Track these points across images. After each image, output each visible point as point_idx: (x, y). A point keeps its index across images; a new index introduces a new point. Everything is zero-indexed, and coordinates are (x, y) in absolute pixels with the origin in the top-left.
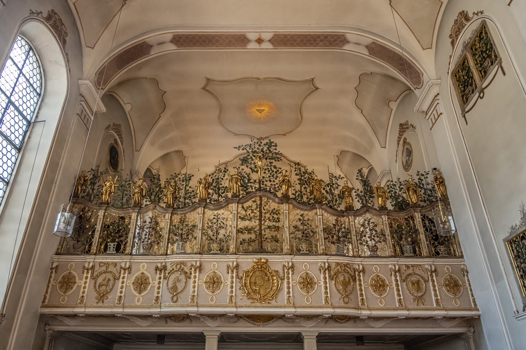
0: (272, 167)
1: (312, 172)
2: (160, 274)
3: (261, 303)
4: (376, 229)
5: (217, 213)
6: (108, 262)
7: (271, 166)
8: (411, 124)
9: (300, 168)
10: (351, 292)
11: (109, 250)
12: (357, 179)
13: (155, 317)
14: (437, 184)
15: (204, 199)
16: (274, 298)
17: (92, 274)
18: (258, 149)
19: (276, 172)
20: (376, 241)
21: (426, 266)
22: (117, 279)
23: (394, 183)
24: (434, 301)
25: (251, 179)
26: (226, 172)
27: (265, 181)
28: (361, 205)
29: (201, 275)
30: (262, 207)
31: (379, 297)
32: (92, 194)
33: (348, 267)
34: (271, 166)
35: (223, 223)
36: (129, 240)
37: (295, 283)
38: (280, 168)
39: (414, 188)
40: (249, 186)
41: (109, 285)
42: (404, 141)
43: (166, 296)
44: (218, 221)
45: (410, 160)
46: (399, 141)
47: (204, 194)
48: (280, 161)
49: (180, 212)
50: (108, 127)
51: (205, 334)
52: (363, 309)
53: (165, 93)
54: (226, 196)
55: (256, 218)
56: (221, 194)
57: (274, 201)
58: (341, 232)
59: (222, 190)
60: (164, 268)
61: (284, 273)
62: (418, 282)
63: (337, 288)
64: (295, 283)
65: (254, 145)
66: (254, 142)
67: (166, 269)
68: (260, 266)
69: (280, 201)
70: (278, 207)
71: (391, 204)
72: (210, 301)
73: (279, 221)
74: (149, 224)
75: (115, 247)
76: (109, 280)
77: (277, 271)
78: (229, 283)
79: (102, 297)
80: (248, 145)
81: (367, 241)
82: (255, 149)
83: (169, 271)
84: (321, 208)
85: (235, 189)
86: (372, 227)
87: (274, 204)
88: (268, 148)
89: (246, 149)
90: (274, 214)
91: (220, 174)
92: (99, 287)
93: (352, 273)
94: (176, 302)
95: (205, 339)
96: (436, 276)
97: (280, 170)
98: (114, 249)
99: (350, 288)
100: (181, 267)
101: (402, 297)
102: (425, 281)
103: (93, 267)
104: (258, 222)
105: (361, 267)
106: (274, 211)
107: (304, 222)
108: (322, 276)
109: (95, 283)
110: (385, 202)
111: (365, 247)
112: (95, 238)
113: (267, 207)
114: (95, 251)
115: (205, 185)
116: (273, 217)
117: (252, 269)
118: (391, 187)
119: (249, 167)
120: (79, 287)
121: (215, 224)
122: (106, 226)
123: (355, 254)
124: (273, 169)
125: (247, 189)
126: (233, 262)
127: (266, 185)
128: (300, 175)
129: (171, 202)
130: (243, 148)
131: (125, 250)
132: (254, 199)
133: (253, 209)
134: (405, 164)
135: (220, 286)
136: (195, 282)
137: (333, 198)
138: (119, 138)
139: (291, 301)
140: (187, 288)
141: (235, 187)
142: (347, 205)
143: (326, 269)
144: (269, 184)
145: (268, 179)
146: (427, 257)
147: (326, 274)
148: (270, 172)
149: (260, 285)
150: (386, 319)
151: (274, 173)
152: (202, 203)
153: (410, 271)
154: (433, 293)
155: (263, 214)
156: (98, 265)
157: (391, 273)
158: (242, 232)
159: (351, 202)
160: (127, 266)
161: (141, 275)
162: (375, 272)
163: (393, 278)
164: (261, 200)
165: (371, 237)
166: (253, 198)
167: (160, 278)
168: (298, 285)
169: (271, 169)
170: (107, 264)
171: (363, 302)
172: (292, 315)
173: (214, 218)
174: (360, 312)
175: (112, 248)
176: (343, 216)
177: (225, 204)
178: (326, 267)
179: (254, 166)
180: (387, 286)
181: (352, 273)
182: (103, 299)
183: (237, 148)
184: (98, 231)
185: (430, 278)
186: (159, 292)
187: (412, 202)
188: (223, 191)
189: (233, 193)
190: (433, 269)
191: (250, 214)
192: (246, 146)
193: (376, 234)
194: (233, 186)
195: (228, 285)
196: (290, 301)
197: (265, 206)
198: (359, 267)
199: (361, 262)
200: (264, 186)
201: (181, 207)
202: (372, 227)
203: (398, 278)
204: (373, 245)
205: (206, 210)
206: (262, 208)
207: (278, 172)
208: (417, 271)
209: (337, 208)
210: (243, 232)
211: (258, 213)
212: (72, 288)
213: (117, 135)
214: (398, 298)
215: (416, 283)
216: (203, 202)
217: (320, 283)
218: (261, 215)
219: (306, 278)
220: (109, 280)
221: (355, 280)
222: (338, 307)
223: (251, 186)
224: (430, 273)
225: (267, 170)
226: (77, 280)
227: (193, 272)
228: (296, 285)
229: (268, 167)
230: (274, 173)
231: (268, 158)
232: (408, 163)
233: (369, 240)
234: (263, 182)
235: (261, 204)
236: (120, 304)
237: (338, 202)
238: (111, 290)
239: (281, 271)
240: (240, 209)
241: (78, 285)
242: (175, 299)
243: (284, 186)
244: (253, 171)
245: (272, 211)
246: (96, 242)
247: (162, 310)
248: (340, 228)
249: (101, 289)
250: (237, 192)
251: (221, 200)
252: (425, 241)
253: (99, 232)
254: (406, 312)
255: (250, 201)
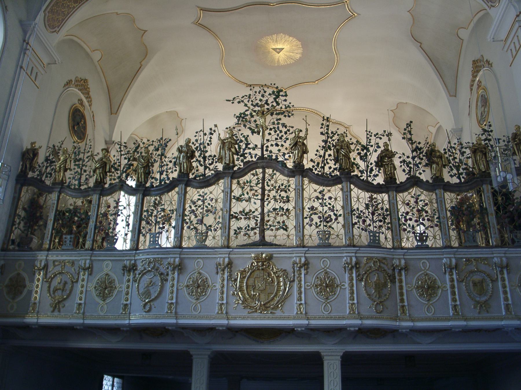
1: (344, 133)
2: (129, 276)
3: (261, 313)
5: (203, 192)
7: (278, 124)
8: (487, 60)
11: (65, 245)
13: (123, 330)
14: (516, 144)
15: (186, 173)
16: (279, 306)
17: (46, 275)
18: (261, 100)
19: (286, 133)
20: (426, 226)
21: (495, 260)
22: (74, 282)
25: (250, 144)
26: (212, 134)
27: (269, 146)
29: (181, 276)
30: (266, 182)
31: (426, 303)
32: (44, 173)
33: (384, 263)
34: (278, 124)
35: (212, 206)
36: (89, 230)
37: (310, 286)
38: (292, 127)
39: (483, 150)
40: (246, 154)
41: (66, 290)
42: (478, 85)
43: (137, 303)
44: (204, 203)
45: (486, 112)
49: (154, 193)
50: (68, 83)
52: (403, 320)
53: (145, 32)
54: (215, 168)
55: (256, 198)
56: (208, 165)
59: (209, 160)
60: (134, 267)
61: (294, 273)
62: (482, 282)
63: (367, 292)
64: (310, 286)
65: (255, 95)
66: (254, 92)
68: (261, 263)
69: (290, 174)
70: (288, 181)
71: (450, 174)
73: (288, 201)
74: (114, 209)
75: (72, 240)
76: (66, 283)
77: (285, 270)
78: (218, 286)
79: (57, 306)
80: (247, 96)
82: (256, 102)
83: (139, 272)
87: (282, 177)
88: (275, 99)
89: (243, 101)
90: (281, 191)
92: (54, 292)
93: (390, 272)
94: (149, 311)
96: (508, 273)
97: (291, 130)
98: (71, 243)
101: (458, 303)
103: (46, 267)
104: (259, 202)
105: (403, 262)
106: (281, 187)
108: (347, 275)
109: (49, 287)
111: (411, 235)
113: (272, 182)
114: (47, 246)
115: (187, 153)
116: (280, 195)
117: (249, 267)
118: (449, 150)
119: (248, 126)
121: (200, 206)
122: (61, 214)
123: (396, 244)
124: (281, 128)
125: (245, 158)
126: (224, 258)
127: (271, 152)
129: (143, 180)
130: (239, 100)
132: (254, 171)
133: (252, 185)
134: (479, 118)
135: (206, 291)
136: (173, 286)
137: (368, 166)
138: (86, 98)
140: (163, 294)
141: (227, 155)
142: (387, 176)
144: (275, 149)
145: (274, 143)
146: (497, 246)
147: (352, 273)
148: (277, 133)
149: (261, 289)
151: (283, 134)
152: (183, 179)
154: (502, 296)
155: (266, 192)
157: (445, 271)
160: (87, 265)
162: (423, 268)
163: (447, 276)
164: (264, 173)
165: (419, 220)
166: (252, 170)
167: (129, 281)
168: (313, 288)
169: (278, 128)
170: (63, 263)
171: (403, 310)
173: (199, 199)
174: (398, 324)
175: (68, 241)
179: (254, 126)
181: (390, 272)
182: (59, 306)
183: (230, 101)
184: (51, 220)
185: (499, 276)
188: (210, 162)
189: (225, 163)
191: (249, 192)
192: (243, 97)
193: (426, 216)
197: (269, 180)
198: (400, 262)
200: (269, 152)
201: (155, 186)
202: (421, 206)
203: (454, 277)
204: (422, 232)
205: (188, 189)
206: (266, 184)
207: (288, 133)
208: (482, 267)
209: (373, 180)
210: (238, 217)
211: (260, 191)
213: (83, 94)
214: (453, 303)
215: (479, 283)
216: (184, 177)
217: (343, 285)
218: (263, 194)
219: (325, 279)
220: (66, 283)
221: (393, 281)
222: (368, 318)
223: (250, 153)
224: (500, 269)
225: (273, 130)
227: (170, 273)
228: (311, 288)
229: (274, 126)
230: (283, 134)
231: (275, 113)
233: (415, 224)
234: (267, 147)
235: (264, 178)
236: (79, 313)
237: (373, 173)
238: (68, 296)
239: (290, 270)
240: (234, 186)
242: (147, 308)
243: (297, 151)
245: (279, 187)
246: (48, 234)
248: (374, 209)
249: (56, 294)
251: (208, 174)
253: (52, 222)
254: (463, 323)
255: (249, 174)
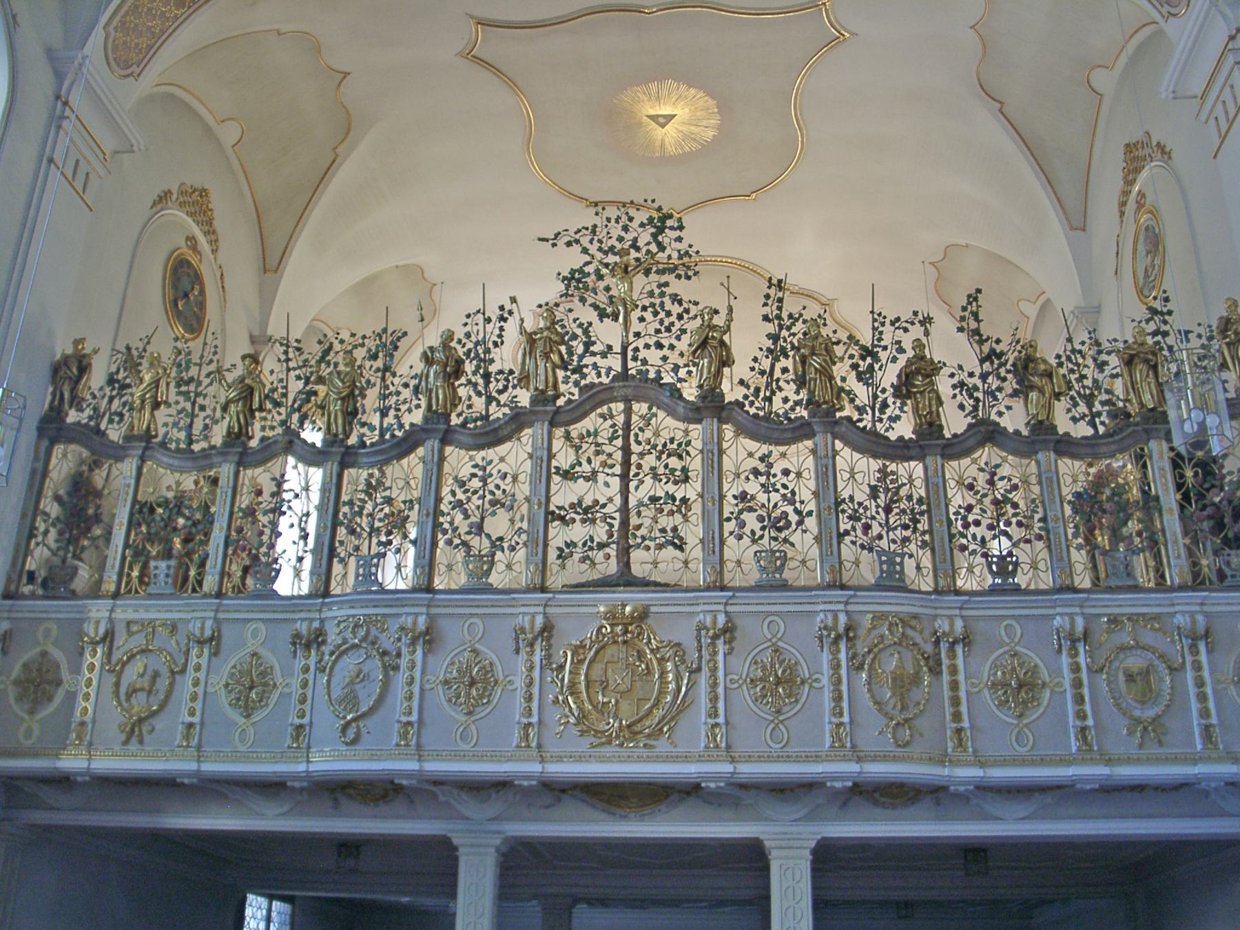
0: (667, 300)
1: (820, 316)
3: (621, 745)
4: (1015, 500)
5: (483, 459)
6: (152, 621)
7: (662, 294)
8: (1158, 144)
9: (780, 300)
10: (921, 707)
11: (155, 583)
12: (961, 330)
14: (1228, 344)
15: (442, 414)
16: (665, 729)
17: (109, 655)
18: (620, 239)
19: (680, 317)
20: (1015, 539)
21: (1179, 619)
22: (177, 672)
23: (1078, 347)
24: (1197, 731)
25: (594, 343)
28: (969, 420)
29: (430, 658)
30: (632, 433)
35: (504, 491)
37: (737, 681)
38: (696, 304)
40: (587, 366)
42: (1137, 202)
43: (326, 721)
44: (485, 484)
46: (1123, 204)
47: (441, 397)
48: (693, 278)
49: (366, 460)
51: (455, 841)
54: (512, 402)
55: (610, 471)
56: (494, 394)
57: (671, 413)
58: (896, 511)
59: (498, 381)
60: (318, 637)
61: (700, 651)
62: (1146, 672)
63: (873, 697)
64: (737, 681)
65: (606, 226)
66: (604, 219)
67: (324, 642)
68: (620, 627)
70: (686, 432)
71: (1070, 415)
72: (459, 741)
73: (686, 479)
74: (270, 499)
75: (172, 571)
76: (156, 675)
78: (519, 682)
80: (587, 229)
81: (983, 540)
82: (610, 243)
83: (332, 648)
84: (832, 433)
85: (543, 378)
86: (1002, 491)
87: (670, 422)
88: (655, 236)
89: (577, 241)
90: (669, 456)
91: (489, 327)
92: (129, 696)
95: (456, 859)
96: (1210, 651)
97: (694, 310)
98: (170, 580)
99: (917, 694)
100: (368, 632)
102: (1169, 668)
103: (109, 636)
104: (616, 483)
105: (959, 625)
106: (669, 446)
107: (772, 480)
108: (826, 657)
109: (117, 684)
110: (1050, 408)
111: (979, 559)
112: (112, 546)
113: (648, 434)
115: (446, 365)
116: (666, 466)
117: (594, 637)
118: (1069, 359)
119: (590, 301)
120: (71, 697)
121: (475, 492)
122: (145, 510)
123: (942, 583)
125: (584, 376)
127: (645, 362)
128: (776, 322)
129: (340, 429)
130: (569, 239)
131: (200, 583)
132: (605, 409)
133: (600, 440)
134: (1141, 282)
135: (491, 694)
136: (411, 682)
137: (875, 397)
139: (718, 739)
141: (541, 370)
142: (920, 419)
143: (838, 637)
144: (654, 356)
145: (651, 341)
146: (1182, 588)
147: (838, 651)
148: (659, 317)
150: (1037, 794)
151: (673, 318)
152: (434, 426)
153: (1125, 637)
154: (1194, 706)
155: (634, 458)
156: (124, 630)
157: (1060, 646)
158: (562, 518)
159: (934, 409)
160: (208, 633)
161: (249, 660)
162: (1007, 640)
164: (628, 412)
165: (998, 525)
166: (600, 404)
167: (306, 670)
168: (744, 687)
169: (662, 305)
170: (150, 627)
171: (960, 740)
172: (722, 784)
173: (474, 475)
174: (946, 772)
176: (909, 459)
177: (509, 429)
178: (841, 628)
179: (606, 301)
180: (1044, 685)
181: (929, 648)
182: (140, 730)
183: (547, 240)
186: (304, 711)
187: (1142, 405)
188: (500, 386)
189: (536, 389)
190: (1201, 629)
191: (592, 457)
194: (537, 366)
195: (516, 689)
196: (715, 740)
199: (961, 608)
200: (639, 363)
201: (368, 443)
202: (1002, 491)
203: (1082, 659)
204: (1004, 553)
205: (448, 450)
206: (632, 438)
207: (685, 316)
208: (1148, 638)
209: (887, 430)
210: (567, 518)
211: (618, 456)
212: (50, 699)
214: (1079, 723)
216: (438, 422)
218: (626, 464)
219: (772, 665)
220: (156, 675)
221: (935, 670)
223: (595, 366)
224: (1190, 641)
225: (650, 310)
226: (65, 674)
227: (404, 651)
228: (740, 686)
229: (652, 300)
230: (673, 318)
231: (654, 269)
232: (1149, 277)
233: (988, 535)
234: (636, 350)
235: (627, 426)
237: (889, 412)
239: (690, 645)
240: (557, 444)
241: (68, 692)
243: (706, 360)
244: (602, 315)
245: (665, 445)
247: (312, 768)
248: (891, 500)
249: (133, 700)
250: (547, 387)
251: (495, 416)
252: (1180, 536)
253: (124, 529)
254: (1101, 770)
255: (593, 415)
